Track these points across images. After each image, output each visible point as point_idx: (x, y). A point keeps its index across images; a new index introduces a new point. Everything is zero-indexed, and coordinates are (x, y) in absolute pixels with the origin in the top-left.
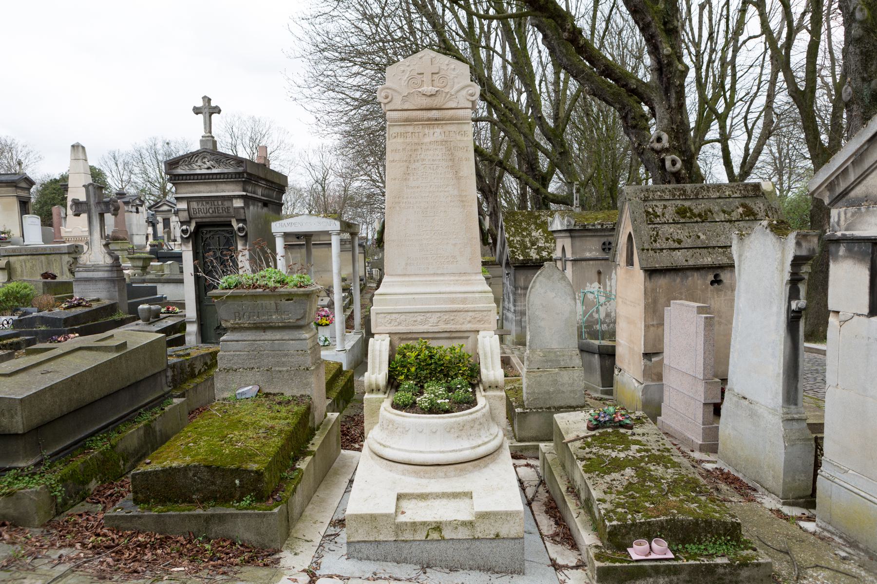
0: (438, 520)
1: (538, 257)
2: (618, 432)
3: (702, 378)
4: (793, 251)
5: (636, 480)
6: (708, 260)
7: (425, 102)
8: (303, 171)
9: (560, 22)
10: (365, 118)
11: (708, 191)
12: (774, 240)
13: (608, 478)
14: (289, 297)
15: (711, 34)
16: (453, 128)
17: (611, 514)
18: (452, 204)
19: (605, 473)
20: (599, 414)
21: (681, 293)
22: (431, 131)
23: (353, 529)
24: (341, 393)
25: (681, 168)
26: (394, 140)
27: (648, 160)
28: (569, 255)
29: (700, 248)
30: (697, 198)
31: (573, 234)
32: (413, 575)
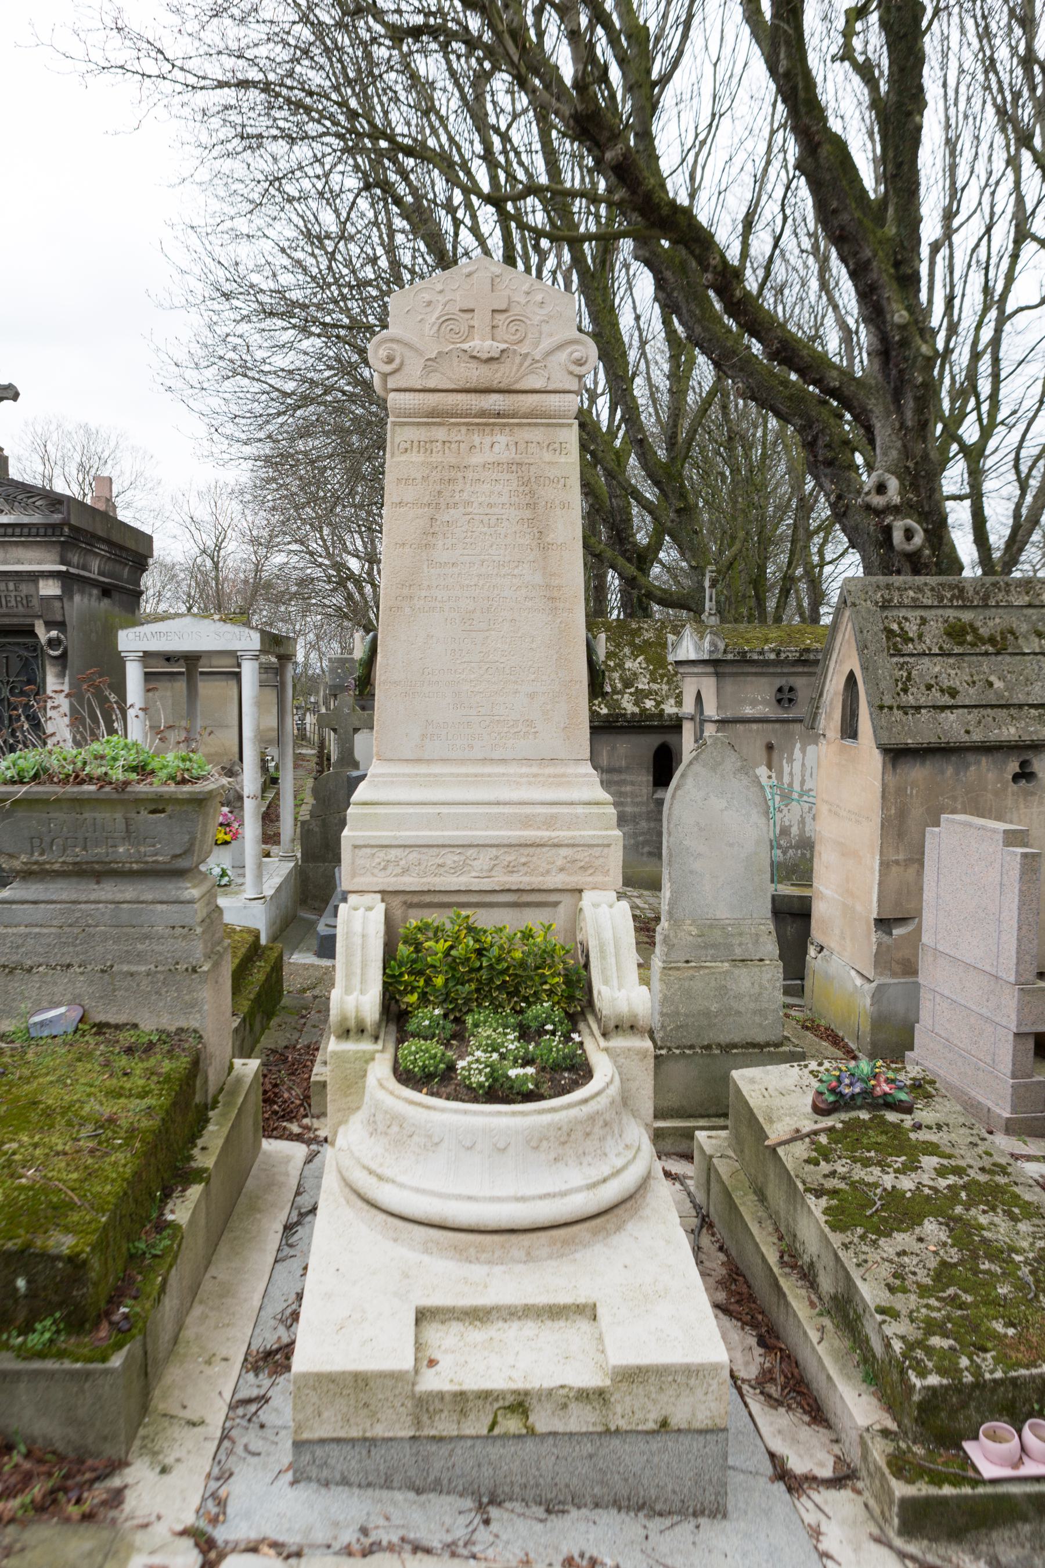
0: (520, 1385)
1: (637, 710)
2: (884, 1122)
5: (953, 1255)
6: (1010, 732)
7: (477, 375)
8: (178, 531)
9: (697, 251)
10: (304, 432)
11: (1008, 592)
13: (888, 1247)
14: (158, 805)
15: (950, 300)
16: (536, 435)
17: (919, 1354)
18: (529, 604)
19: (880, 1233)
20: (839, 1079)
21: (954, 799)
22: (488, 440)
23: (309, 1410)
24: (258, 1001)
25: (923, 546)
26: (404, 458)
27: (856, 528)
28: (711, 710)
29: (992, 706)
30: (986, 606)
31: (721, 670)
32: (460, 1533)
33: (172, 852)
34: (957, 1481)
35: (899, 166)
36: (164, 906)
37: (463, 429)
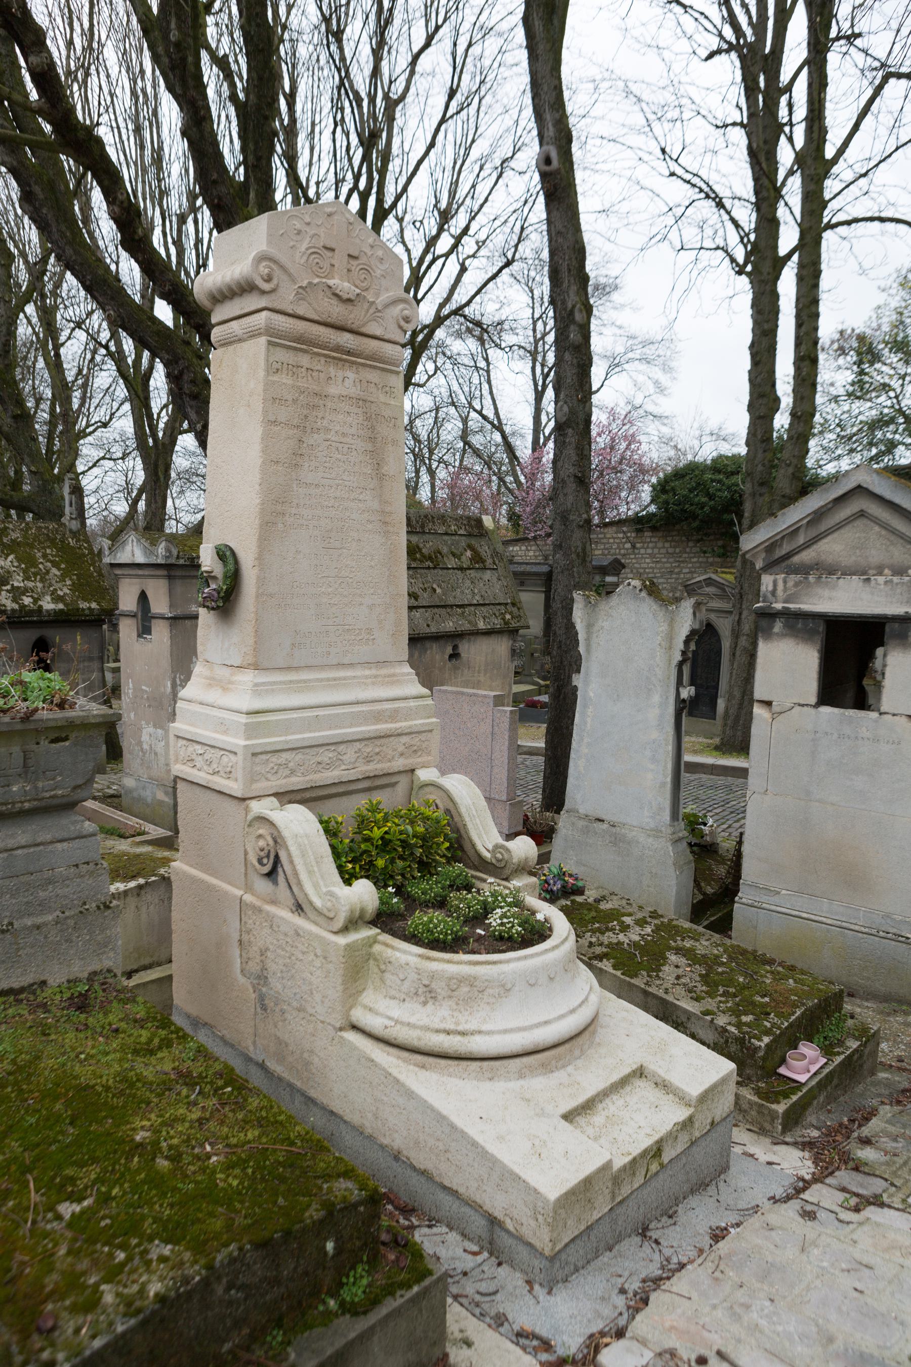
1: (16, 607)
3: (504, 798)
4: (689, 622)
6: (449, 626)
7: (336, 311)
12: (655, 607)
16: (373, 376)
18: (370, 526)
22: (340, 374)
29: (438, 607)
30: (424, 533)
31: (173, 573)
33: (73, 784)
34: (794, 1090)
35: (259, 159)
36: (65, 845)
37: (323, 359)
